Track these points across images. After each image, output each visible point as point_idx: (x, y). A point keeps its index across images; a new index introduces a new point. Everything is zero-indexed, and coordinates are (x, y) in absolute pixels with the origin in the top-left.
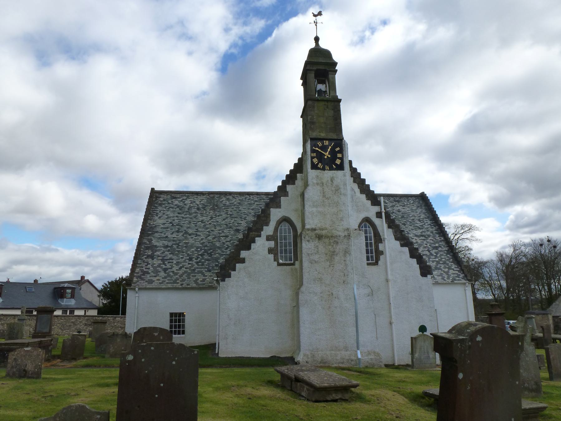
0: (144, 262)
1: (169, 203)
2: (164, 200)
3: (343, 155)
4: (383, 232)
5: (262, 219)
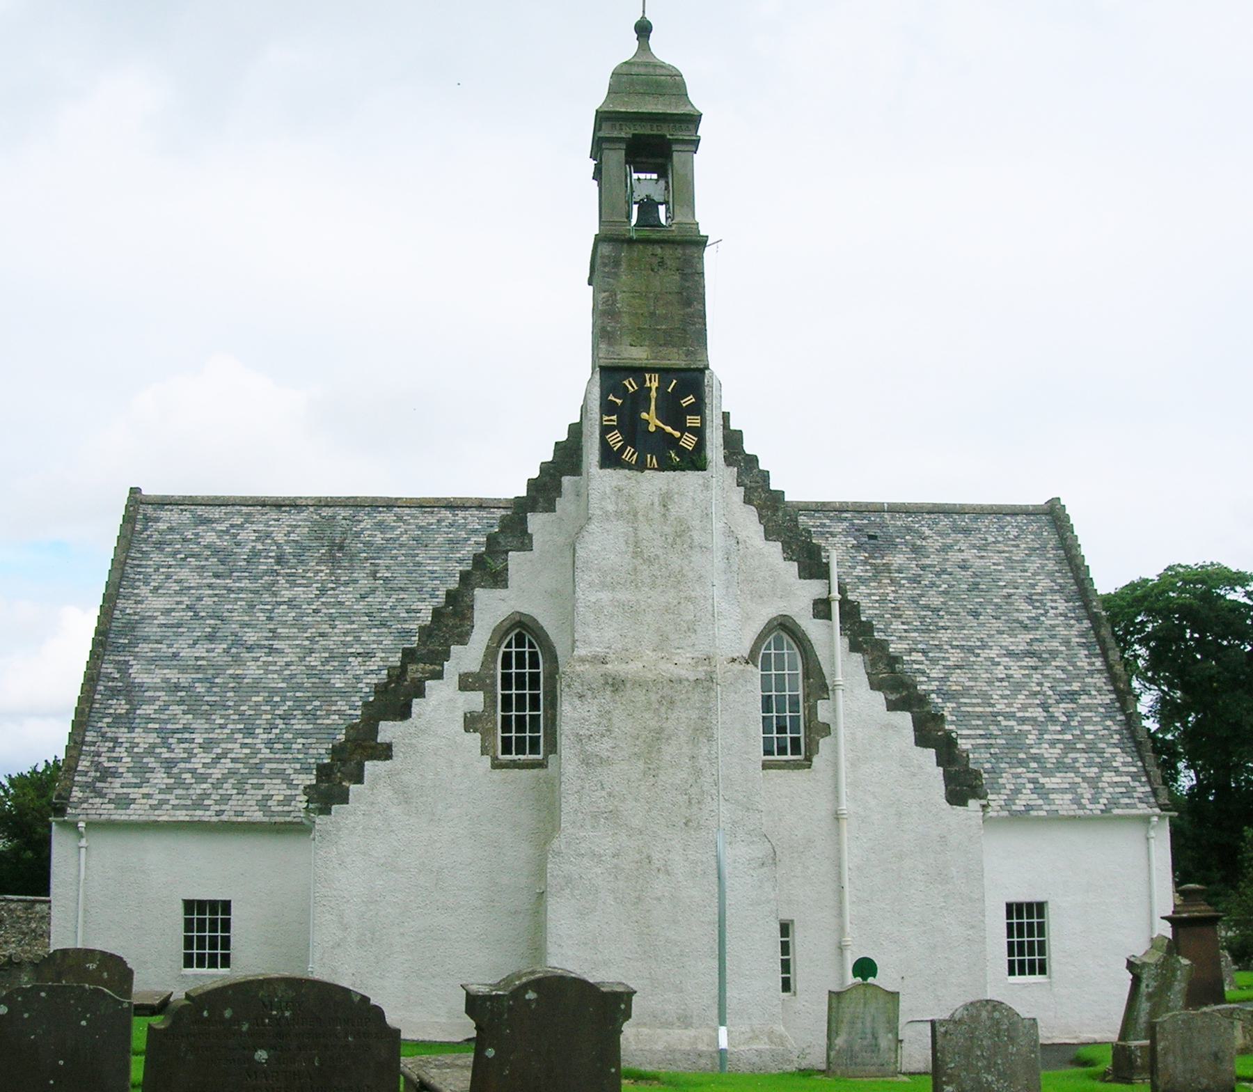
1: (185, 540)
2: (171, 529)
3: (703, 421)
4: (833, 664)
5: (452, 618)
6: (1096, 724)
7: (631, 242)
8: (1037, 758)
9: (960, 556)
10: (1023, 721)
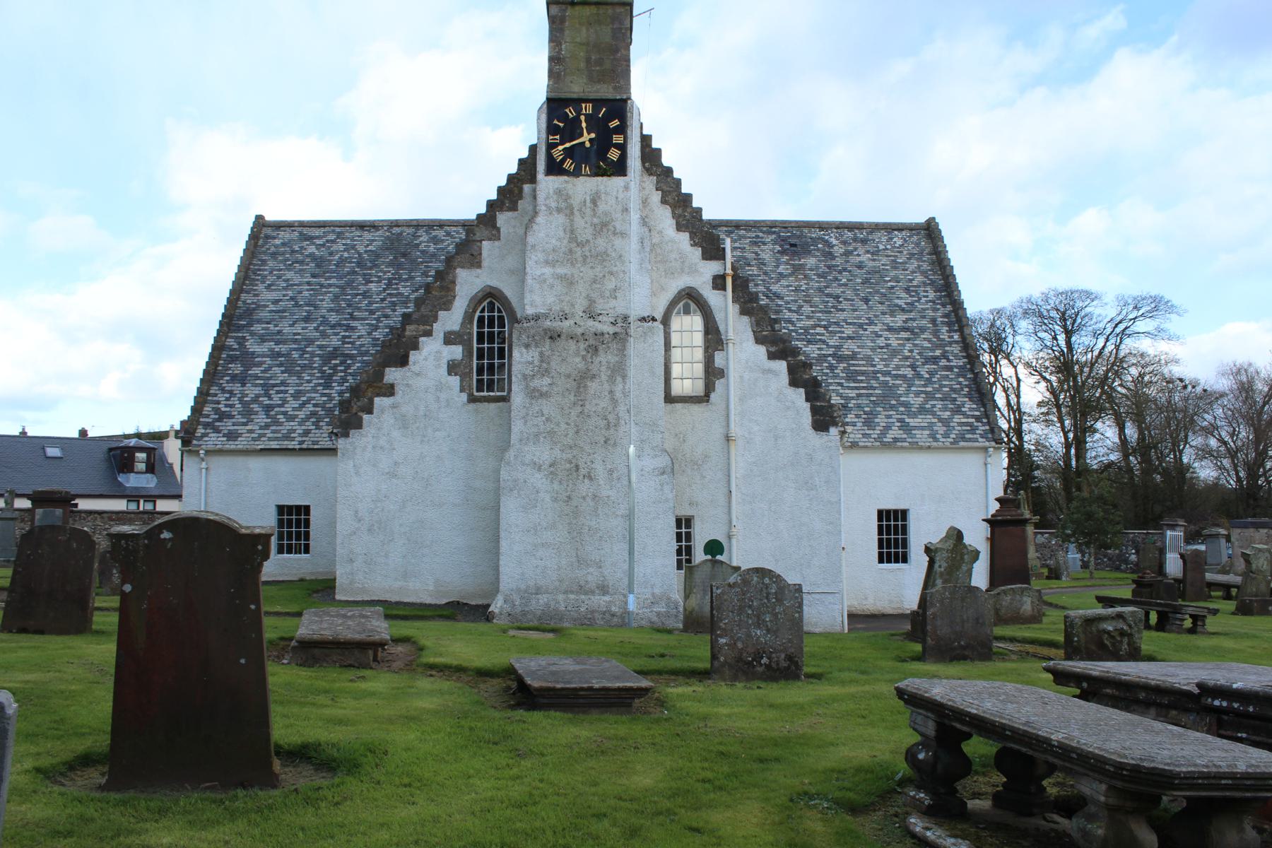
1: (293, 252)
2: (284, 244)
5: (438, 292)
6: (951, 380)
9: (858, 259)
10: (897, 377)
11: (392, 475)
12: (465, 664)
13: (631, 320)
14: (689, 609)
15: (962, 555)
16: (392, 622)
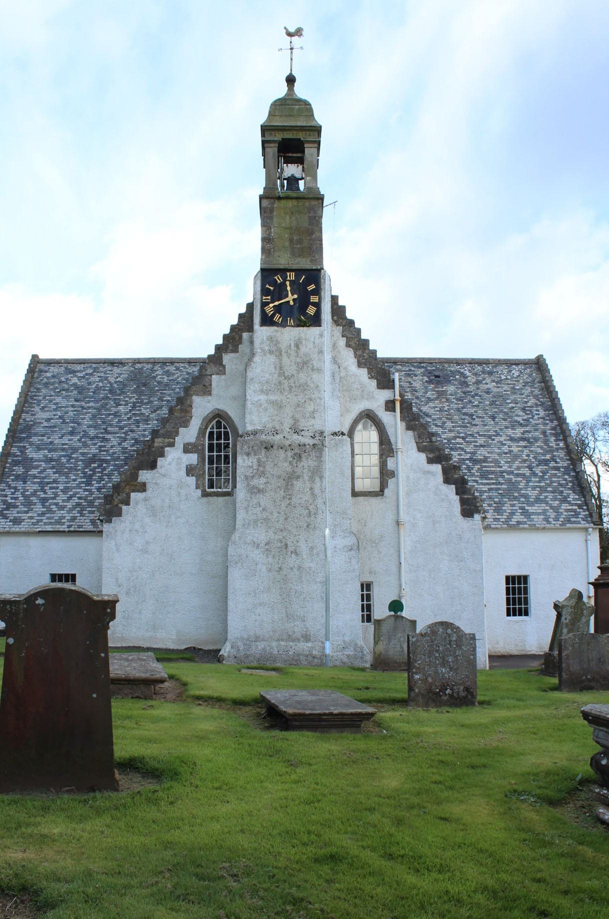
0: (10, 487)
1: (61, 382)
2: (53, 376)
5: (180, 412)
6: (559, 477)
7: (279, 198)
8: (526, 496)
9: (486, 386)
10: (518, 475)
11: (145, 551)
12: (223, 696)
13: (326, 434)
14: (378, 653)
15: (582, 610)
16: (166, 664)
